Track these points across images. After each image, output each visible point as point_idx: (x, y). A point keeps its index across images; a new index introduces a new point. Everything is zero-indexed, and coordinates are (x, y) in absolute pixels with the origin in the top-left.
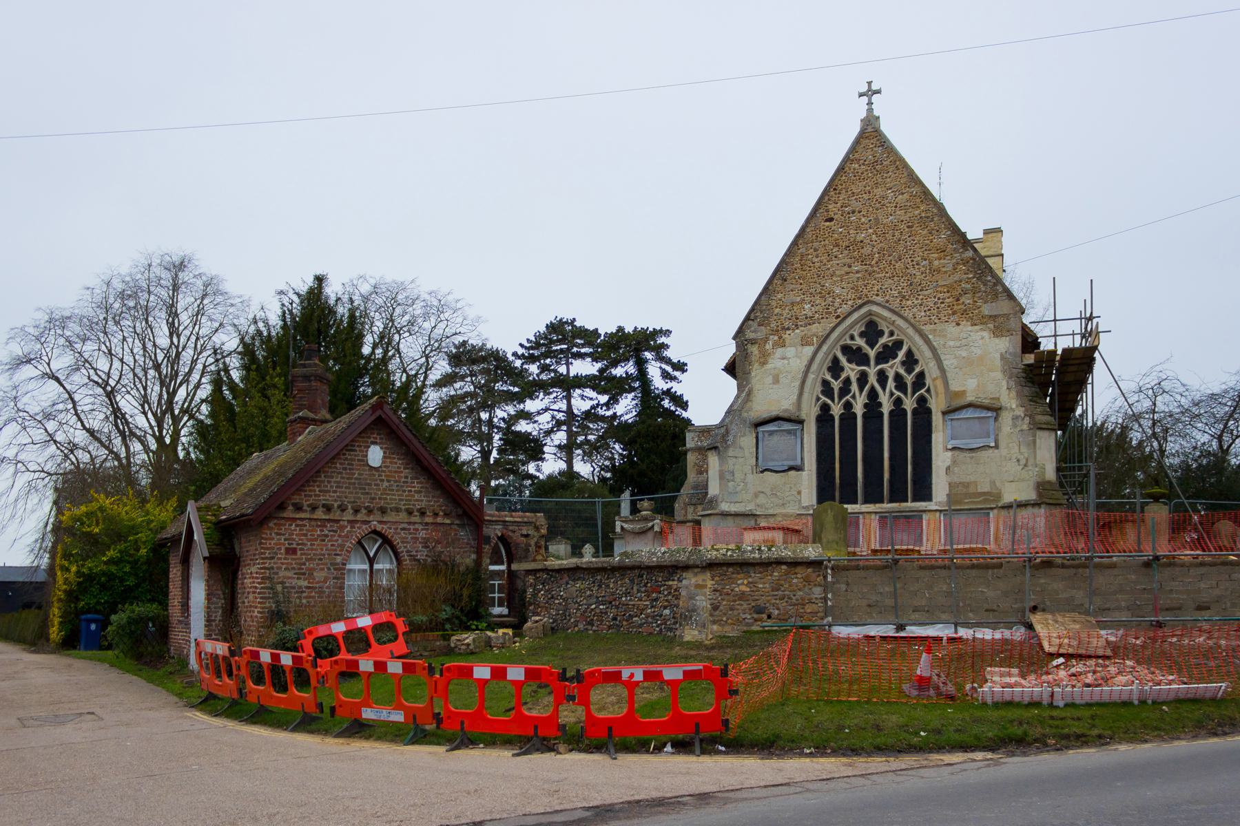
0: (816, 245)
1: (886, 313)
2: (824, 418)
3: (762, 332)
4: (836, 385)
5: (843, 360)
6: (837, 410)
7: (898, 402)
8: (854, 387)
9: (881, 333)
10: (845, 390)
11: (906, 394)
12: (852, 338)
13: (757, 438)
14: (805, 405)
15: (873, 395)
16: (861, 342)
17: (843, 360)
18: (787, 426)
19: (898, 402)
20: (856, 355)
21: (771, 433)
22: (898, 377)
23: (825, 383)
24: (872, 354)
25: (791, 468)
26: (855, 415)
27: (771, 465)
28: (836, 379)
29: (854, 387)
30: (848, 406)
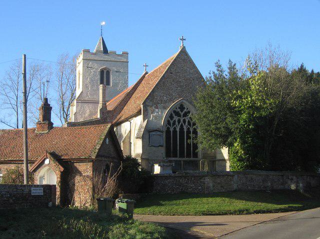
0: (167, 79)
1: (187, 103)
2: (168, 132)
3: (151, 104)
4: (172, 122)
5: (174, 115)
6: (172, 129)
7: (189, 129)
8: (177, 123)
9: (184, 108)
10: (174, 124)
11: (170, 126)
12: (176, 108)
13: (149, 136)
14: (64, 123)
15: (182, 126)
16: (179, 110)
17: (174, 115)
18: (159, 133)
19: (189, 129)
20: (177, 114)
21: (154, 135)
22: (189, 122)
23: (168, 121)
24: (182, 114)
25: (160, 146)
26: (177, 131)
27: (153, 145)
28: (172, 120)
29: (177, 123)
30: (175, 128)
